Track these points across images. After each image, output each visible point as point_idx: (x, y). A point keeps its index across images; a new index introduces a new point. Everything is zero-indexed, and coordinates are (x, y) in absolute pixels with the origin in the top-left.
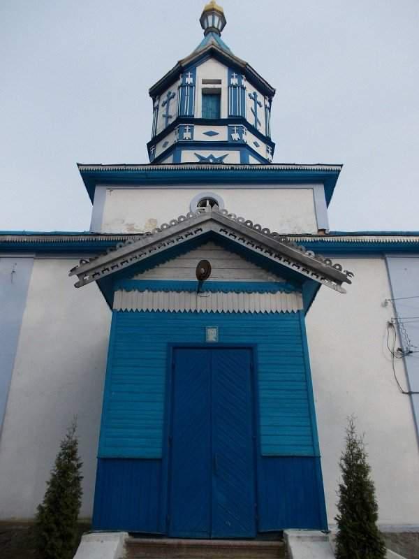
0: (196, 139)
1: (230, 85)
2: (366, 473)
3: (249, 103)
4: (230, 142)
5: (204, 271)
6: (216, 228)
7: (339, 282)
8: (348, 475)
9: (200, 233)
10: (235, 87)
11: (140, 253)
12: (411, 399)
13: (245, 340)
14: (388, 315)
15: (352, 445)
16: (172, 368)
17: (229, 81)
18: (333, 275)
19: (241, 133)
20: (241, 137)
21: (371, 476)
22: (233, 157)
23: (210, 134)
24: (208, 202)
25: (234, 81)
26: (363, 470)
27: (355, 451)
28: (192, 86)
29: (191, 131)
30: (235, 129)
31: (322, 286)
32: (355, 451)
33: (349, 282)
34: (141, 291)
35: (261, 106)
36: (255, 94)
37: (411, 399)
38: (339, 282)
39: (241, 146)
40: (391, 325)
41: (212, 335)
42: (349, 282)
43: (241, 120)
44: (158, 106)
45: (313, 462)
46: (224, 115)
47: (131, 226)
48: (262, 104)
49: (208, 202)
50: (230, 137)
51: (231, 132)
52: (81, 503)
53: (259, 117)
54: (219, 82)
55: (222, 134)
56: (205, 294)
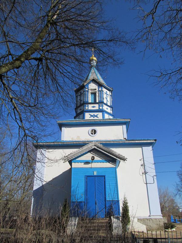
0: (89, 109)
1: (99, 91)
2: (127, 204)
3: (105, 96)
4: (99, 110)
5: (93, 158)
6: (96, 147)
7: (124, 161)
8: (124, 205)
9: (92, 148)
10: (100, 91)
11: (78, 154)
12: (147, 185)
13: (103, 174)
14: (142, 162)
15: (125, 198)
16: (86, 183)
17: (99, 89)
18: (122, 158)
19: (102, 106)
20: (103, 108)
21: (128, 205)
22: (100, 115)
23: (93, 107)
24: (93, 131)
25: (100, 89)
26: (127, 203)
27: (125, 199)
28: (88, 91)
29: (88, 106)
30: (101, 105)
31: (121, 162)
32: (125, 199)
33: (126, 160)
34: (36, 58)
35: (108, 95)
36: (106, 92)
37: (147, 185)
38: (124, 161)
39: (102, 111)
40: (142, 165)
41: (95, 174)
42: (126, 160)
43: (103, 103)
44: (78, 96)
45: (118, 201)
46: (97, 101)
47: (72, 138)
48: (109, 94)
49: (93, 131)
50: (99, 108)
51: (99, 106)
52: (181, 168)
53: (108, 99)
54: (96, 89)
55: (97, 107)
56: (93, 163)
